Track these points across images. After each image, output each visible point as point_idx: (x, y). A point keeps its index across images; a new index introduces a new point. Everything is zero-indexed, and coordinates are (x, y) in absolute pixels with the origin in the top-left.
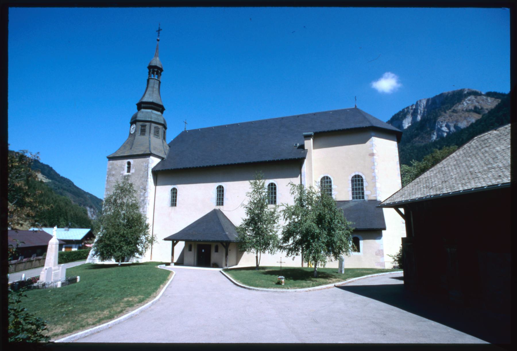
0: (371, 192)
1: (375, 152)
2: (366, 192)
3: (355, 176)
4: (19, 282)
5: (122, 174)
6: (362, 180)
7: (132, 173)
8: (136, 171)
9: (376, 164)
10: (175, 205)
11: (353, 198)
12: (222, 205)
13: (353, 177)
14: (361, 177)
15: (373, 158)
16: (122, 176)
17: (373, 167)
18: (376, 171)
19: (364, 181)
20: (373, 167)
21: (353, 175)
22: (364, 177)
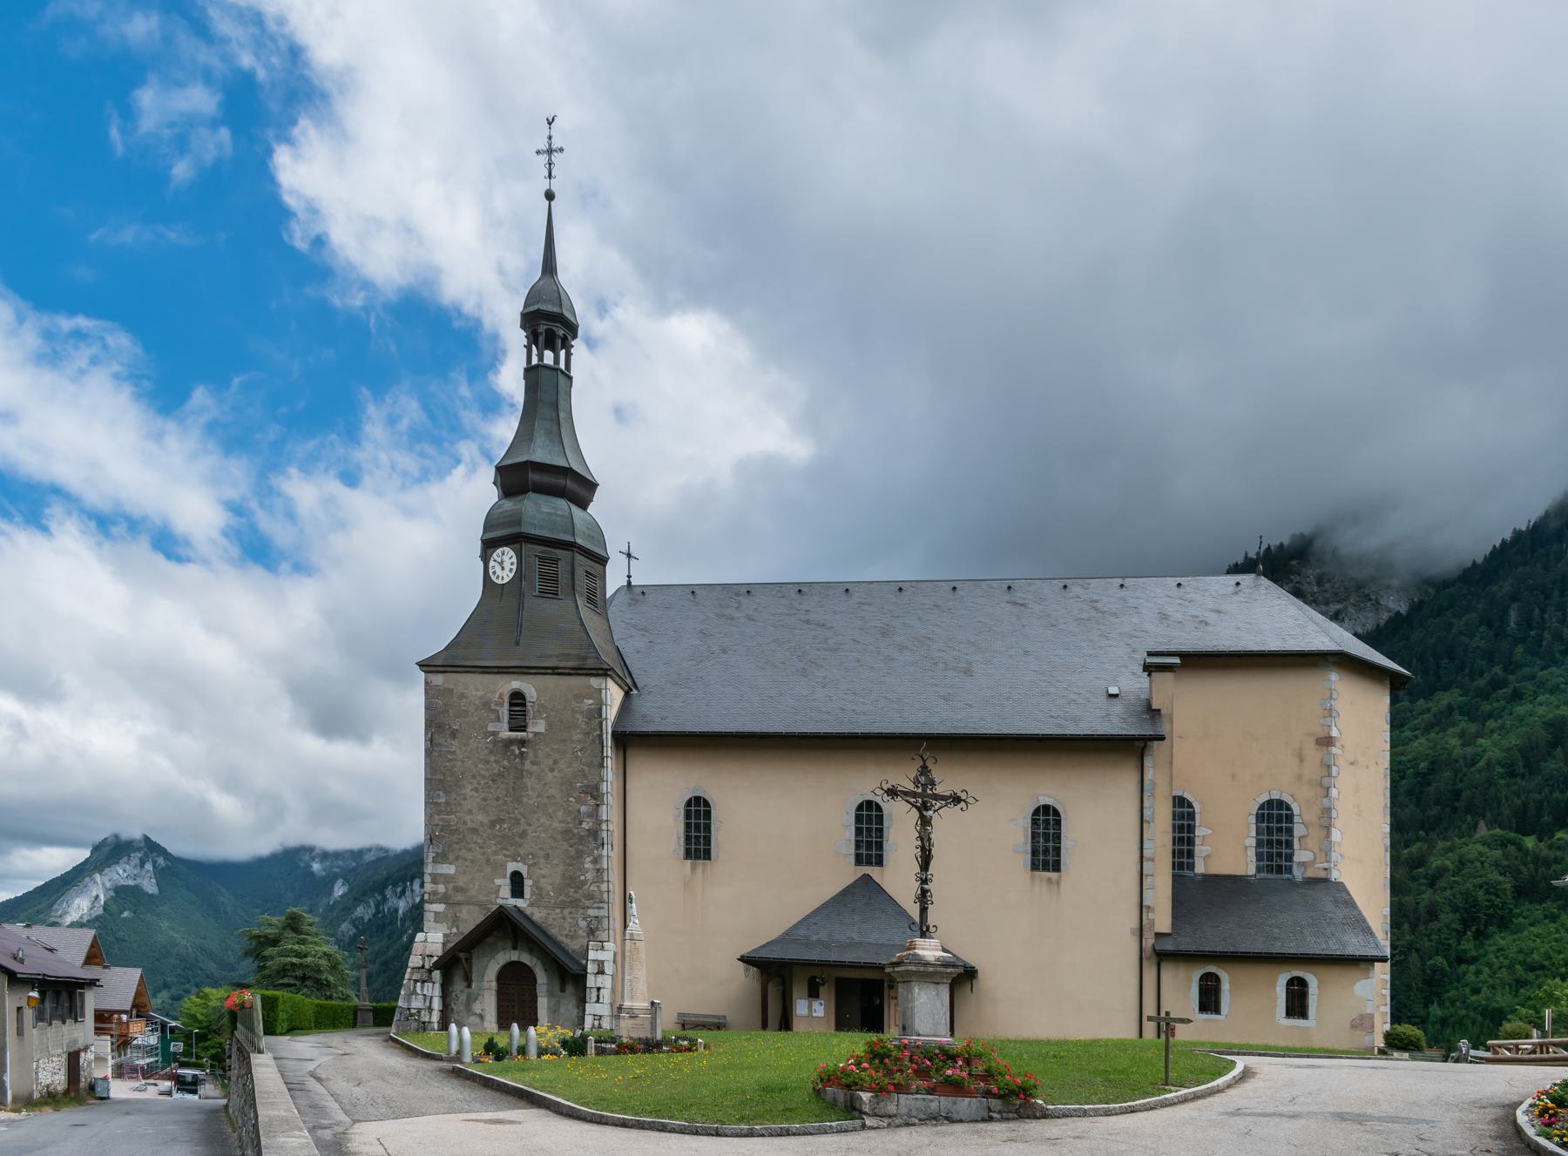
0: (1315, 858)
1: (1334, 733)
2: (1301, 855)
3: (1270, 803)
4: (536, 994)
5: (494, 734)
6: (1290, 818)
7: (536, 734)
8: (550, 726)
9: (1334, 770)
10: (707, 855)
11: (1259, 869)
13: (1262, 807)
14: (1288, 808)
15: (1329, 753)
16: (494, 742)
17: (1325, 781)
18: (1334, 792)
19: (1296, 819)
20: (1325, 781)
21: (1264, 798)
22: (1296, 809)
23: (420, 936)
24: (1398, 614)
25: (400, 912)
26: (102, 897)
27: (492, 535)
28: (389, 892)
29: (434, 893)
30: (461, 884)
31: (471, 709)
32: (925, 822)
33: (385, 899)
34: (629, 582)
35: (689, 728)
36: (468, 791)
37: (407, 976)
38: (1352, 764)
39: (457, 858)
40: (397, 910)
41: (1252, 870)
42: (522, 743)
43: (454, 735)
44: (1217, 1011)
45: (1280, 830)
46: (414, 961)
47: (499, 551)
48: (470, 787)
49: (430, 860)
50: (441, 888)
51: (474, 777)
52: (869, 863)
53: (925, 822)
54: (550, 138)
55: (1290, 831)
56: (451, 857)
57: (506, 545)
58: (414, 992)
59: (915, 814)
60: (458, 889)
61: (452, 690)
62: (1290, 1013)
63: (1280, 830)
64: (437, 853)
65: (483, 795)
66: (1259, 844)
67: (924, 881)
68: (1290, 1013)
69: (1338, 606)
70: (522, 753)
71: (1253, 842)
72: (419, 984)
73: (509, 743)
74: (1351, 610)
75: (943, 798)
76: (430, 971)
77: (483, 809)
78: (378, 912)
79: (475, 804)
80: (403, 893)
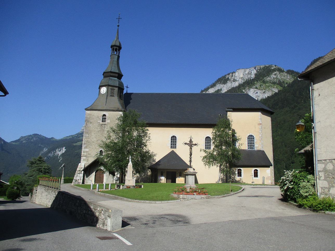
5: (99, 123)
6: (254, 138)
8: (111, 121)
11: (248, 148)
12: (175, 148)
14: (253, 137)
16: (99, 124)
23: (80, 164)
24: (276, 92)
25: (59, 155)
27: (101, 85)
28: (57, 150)
29: (84, 155)
30: (89, 153)
31: (95, 118)
32: (191, 149)
33: (56, 152)
34: (127, 92)
36: (92, 134)
37: (76, 172)
38: (264, 128)
39: (89, 148)
40: (58, 154)
41: (247, 148)
42: (105, 124)
43: (91, 123)
45: (252, 141)
46: (78, 169)
47: (103, 88)
48: (93, 133)
49: (83, 148)
50: (85, 154)
51: (94, 131)
52: (173, 148)
53: (191, 149)
54: (119, 16)
55: (254, 141)
56: (88, 147)
57: (104, 87)
58: (78, 176)
59: (189, 147)
60: (89, 154)
61: (91, 114)
62: (255, 176)
63: (252, 141)
64: (85, 147)
65: (96, 135)
66: (248, 143)
67: (191, 158)
68: (255, 176)
69: (264, 91)
70: (104, 126)
71: (247, 143)
72: (79, 174)
73: (102, 125)
74: (267, 91)
75: (194, 144)
76: (81, 171)
77: (96, 138)
78: (54, 155)
79: (94, 137)
80: (60, 150)
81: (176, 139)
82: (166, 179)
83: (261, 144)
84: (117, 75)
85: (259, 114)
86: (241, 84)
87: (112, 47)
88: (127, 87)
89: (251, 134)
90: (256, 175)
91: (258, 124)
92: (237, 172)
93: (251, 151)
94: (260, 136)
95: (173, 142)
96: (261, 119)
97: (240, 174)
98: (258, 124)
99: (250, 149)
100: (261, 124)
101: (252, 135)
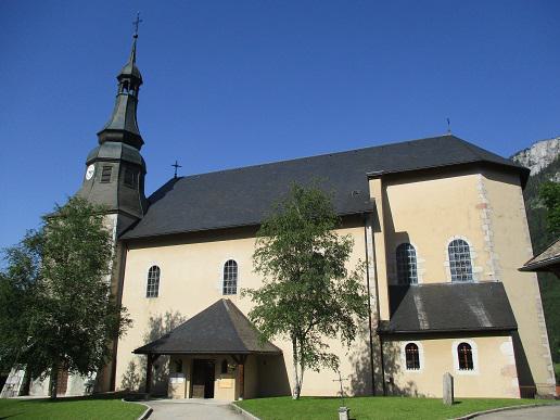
6: (467, 249)
14: (465, 244)
26: (137, 362)
35: (163, 232)
41: (449, 280)
44: (471, 366)
45: (462, 256)
52: (230, 293)
55: (468, 256)
62: (462, 366)
66: (452, 265)
81: (236, 269)
82: (188, 383)
83: (490, 262)
84: (121, 135)
85: (476, 179)
86: (545, 169)
87: (119, 78)
88: (176, 166)
89: (457, 238)
90: (466, 360)
91: (478, 207)
92: (403, 357)
93: (463, 285)
94: (487, 239)
95: (231, 276)
96: (485, 192)
97: (413, 360)
98: (478, 207)
99: (460, 282)
100: (485, 206)
101: (461, 241)
